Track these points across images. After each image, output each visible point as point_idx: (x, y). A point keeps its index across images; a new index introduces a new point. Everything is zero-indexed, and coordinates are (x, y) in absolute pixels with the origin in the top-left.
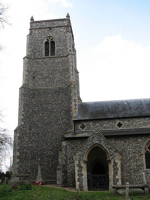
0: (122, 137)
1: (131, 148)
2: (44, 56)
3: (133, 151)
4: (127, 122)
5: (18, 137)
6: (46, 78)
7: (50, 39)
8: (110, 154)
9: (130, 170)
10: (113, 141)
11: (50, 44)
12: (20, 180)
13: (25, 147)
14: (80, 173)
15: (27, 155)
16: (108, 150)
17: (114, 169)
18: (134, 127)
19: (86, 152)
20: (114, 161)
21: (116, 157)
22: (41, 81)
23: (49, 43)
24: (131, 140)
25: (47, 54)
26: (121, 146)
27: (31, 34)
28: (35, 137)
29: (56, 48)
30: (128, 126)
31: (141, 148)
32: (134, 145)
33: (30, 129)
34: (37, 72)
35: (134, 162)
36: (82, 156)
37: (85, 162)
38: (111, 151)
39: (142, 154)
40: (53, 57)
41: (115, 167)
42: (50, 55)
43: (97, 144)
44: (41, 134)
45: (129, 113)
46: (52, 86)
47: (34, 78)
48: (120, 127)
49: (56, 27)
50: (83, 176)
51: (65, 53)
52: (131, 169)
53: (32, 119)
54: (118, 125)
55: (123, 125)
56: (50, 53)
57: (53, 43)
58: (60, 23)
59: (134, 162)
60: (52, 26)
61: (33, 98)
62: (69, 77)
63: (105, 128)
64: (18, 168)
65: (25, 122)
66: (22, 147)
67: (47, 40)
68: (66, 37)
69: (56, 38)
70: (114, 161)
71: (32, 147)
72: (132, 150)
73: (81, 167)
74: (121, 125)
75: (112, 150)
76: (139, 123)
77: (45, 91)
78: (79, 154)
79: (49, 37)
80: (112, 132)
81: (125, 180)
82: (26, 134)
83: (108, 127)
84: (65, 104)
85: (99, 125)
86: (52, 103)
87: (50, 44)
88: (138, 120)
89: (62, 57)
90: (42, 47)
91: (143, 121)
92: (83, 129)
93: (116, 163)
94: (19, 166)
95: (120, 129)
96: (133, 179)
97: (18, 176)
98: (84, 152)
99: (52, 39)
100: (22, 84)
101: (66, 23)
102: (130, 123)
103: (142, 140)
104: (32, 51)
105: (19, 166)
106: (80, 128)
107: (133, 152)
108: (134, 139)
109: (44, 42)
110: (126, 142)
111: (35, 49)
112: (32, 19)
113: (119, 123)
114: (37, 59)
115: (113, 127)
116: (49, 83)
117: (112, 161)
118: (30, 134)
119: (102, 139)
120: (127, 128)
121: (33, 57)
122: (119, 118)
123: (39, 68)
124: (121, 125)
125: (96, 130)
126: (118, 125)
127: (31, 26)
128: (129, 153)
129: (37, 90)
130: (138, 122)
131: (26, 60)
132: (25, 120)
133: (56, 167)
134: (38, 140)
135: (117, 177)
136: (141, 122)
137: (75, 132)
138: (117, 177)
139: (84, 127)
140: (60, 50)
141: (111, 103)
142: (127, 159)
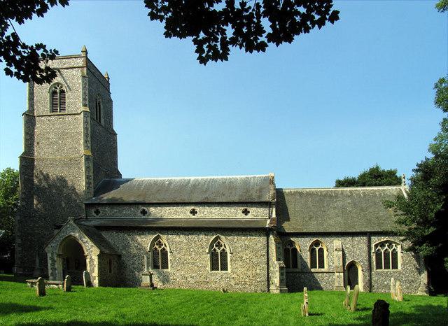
37: (59, 256)
49: (67, 68)
54: (141, 212)
60: (60, 67)
63: (125, 215)
73: (54, 261)
77: (54, 160)
80: (179, 222)
83: (129, 215)
95: (143, 217)
106: (94, 214)
115: (257, 212)
126: (141, 212)
133: (399, 280)
137: (87, 218)
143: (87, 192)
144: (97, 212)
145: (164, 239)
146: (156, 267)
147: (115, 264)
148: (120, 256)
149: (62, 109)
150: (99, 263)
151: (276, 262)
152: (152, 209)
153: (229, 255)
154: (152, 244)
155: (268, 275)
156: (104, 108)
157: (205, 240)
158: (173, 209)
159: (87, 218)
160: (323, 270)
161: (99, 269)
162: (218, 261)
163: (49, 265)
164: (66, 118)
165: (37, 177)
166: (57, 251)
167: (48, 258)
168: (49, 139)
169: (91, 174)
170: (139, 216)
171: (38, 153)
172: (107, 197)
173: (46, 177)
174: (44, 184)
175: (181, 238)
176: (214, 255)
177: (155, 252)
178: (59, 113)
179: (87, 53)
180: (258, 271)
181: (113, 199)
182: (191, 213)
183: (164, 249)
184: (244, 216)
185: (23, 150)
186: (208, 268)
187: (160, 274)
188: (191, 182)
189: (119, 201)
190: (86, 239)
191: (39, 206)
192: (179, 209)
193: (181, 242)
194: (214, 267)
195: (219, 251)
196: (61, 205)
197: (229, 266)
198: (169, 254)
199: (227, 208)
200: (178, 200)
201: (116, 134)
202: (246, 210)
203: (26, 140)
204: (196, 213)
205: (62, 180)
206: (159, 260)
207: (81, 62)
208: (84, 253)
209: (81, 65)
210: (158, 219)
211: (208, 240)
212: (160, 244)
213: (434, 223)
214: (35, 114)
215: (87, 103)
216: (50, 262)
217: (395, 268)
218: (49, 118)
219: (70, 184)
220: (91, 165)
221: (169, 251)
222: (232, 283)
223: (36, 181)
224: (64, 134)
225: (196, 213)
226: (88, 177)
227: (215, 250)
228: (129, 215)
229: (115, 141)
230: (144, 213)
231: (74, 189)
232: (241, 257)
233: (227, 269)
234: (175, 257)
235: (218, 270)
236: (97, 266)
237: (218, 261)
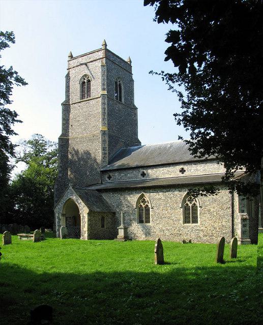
37: (63, 215)
49: (90, 62)
54: (142, 175)
77: (82, 138)
80: (201, 178)
126: (142, 175)
137: (102, 183)
143: (103, 161)
144: (109, 178)
145: (147, 196)
146: (141, 221)
147: (108, 220)
148: (114, 213)
149: (89, 95)
150: (89, 220)
151: (239, 214)
152: (150, 171)
154: (138, 202)
155: (233, 227)
156: (125, 87)
157: (179, 195)
158: (165, 169)
161: (89, 225)
162: (190, 215)
163: (57, 222)
164: (91, 102)
165: (71, 153)
166: (61, 211)
169: (107, 146)
170: (140, 178)
171: (72, 134)
172: (118, 164)
173: (77, 152)
174: (75, 157)
175: (160, 195)
176: (186, 209)
177: (140, 208)
178: (86, 99)
179: (106, 45)
180: (224, 223)
181: (123, 165)
182: (180, 171)
183: (147, 206)
184: (181, 175)
185: (60, 133)
186: (181, 222)
187: (144, 227)
189: (126, 167)
190: (80, 201)
191: (72, 176)
192: (171, 169)
193: (160, 199)
194: (186, 220)
195: (190, 205)
196: (86, 174)
197: (199, 219)
198: (151, 210)
199: (210, 164)
200: (170, 161)
203: (63, 124)
204: (185, 171)
205: (88, 153)
206: (143, 216)
207: (101, 54)
210: (154, 179)
211: (181, 195)
212: (144, 201)
214: (70, 103)
215: (105, 87)
216: (57, 220)
218: (79, 104)
219: (93, 155)
220: (107, 138)
221: (198, 206)
222: (201, 234)
223: (70, 156)
224: (90, 115)
225: (185, 171)
226: (104, 149)
227: (187, 204)
229: (136, 115)
230: (143, 175)
231: (95, 160)
232: (209, 211)
234: (155, 212)
235: (189, 222)
236: (87, 222)
237: (190, 215)
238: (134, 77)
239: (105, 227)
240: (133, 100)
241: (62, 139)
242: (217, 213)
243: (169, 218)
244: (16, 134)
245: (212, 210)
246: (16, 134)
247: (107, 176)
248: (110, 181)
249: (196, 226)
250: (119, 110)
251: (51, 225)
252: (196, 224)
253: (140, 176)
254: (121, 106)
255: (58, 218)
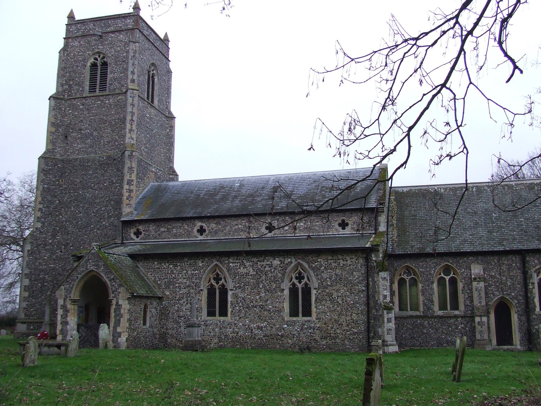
0: (172, 258)
1: (184, 278)
2: (86, 94)
3: (186, 283)
4: (214, 226)
5: (28, 251)
6: (87, 136)
7: (99, 56)
8: (112, 289)
9: (179, 317)
10: (156, 263)
11: (99, 67)
12: (28, 328)
13: (42, 271)
14: (64, 320)
15: (46, 284)
16: (108, 283)
17: (115, 316)
18: (225, 234)
19: (76, 283)
20: (117, 303)
21: (120, 295)
22: (78, 144)
23: (97, 66)
24: (186, 263)
25: (92, 88)
26: (168, 273)
27: (66, 45)
28: (61, 252)
29: (110, 76)
30: (216, 232)
31: (201, 278)
32: (189, 272)
33: (54, 236)
34: (72, 126)
35: (187, 303)
36: (68, 291)
38: (114, 283)
39: (202, 290)
40: (102, 96)
41: (118, 313)
42: (97, 90)
43: (92, 271)
44: (71, 247)
45: (227, 206)
46: (96, 153)
47: (66, 137)
48: (201, 235)
49: (112, 32)
50: (68, 326)
51: (123, 86)
52: (181, 317)
53: (57, 218)
54: (198, 231)
55: (207, 232)
56: (98, 87)
57: (105, 64)
58: (120, 24)
59: (187, 303)
61: (61, 176)
62: (124, 136)
64: (25, 308)
65: (43, 223)
66: (35, 269)
67: (96, 59)
68: (128, 52)
69: (110, 53)
70: (117, 303)
71: (54, 269)
72: (185, 281)
73: (66, 311)
74: (205, 231)
75: (116, 282)
76: (236, 227)
78: (65, 288)
79: (98, 53)
81: (169, 336)
82: (45, 245)
84: (116, 188)
85: (166, 230)
86: (94, 186)
87: (99, 67)
88: (235, 223)
89: (118, 94)
90: (83, 74)
91: (244, 224)
92: (137, 237)
93: (120, 305)
94: (27, 305)
95: (201, 238)
96: (182, 333)
97: (24, 323)
98: (73, 285)
99: (104, 58)
100: (45, 150)
101: (130, 22)
102: (220, 227)
103: (204, 264)
104: (67, 83)
105: (27, 305)
106: (133, 236)
107: (187, 284)
108: (192, 261)
109: (89, 64)
110: (177, 266)
111: (71, 79)
112: (71, 16)
113: (201, 227)
114: (73, 99)
116: (91, 146)
117: (114, 302)
118: (53, 246)
119: (100, 263)
120: (213, 237)
121: (66, 96)
122: (200, 218)
123: (75, 117)
124: (205, 231)
125: (93, 248)
126: (198, 231)
127: (68, 31)
128: (180, 286)
129: (69, 161)
130: (234, 226)
131: (53, 102)
132: (45, 219)
134: (66, 256)
135: (119, 330)
136: (240, 226)
138: (119, 330)
139: (141, 233)
140: (115, 80)
141: (214, 181)
142: (175, 297)
144: (138, 234)
149: (103, 88)
153: (314, 292)
159: (122, 243)
160: (456, 312)
167: (59, 307)
168: (81, 130)
180: (355, 317)
183: (223, 285)
188: (270, 182)
193: (247, 274)
197: (314, 309)
201: (173, 118)
202: (343, 221)
208: (108, 296)
209: (130, 27)
213: (304, 228)
217: (212, 316)
228: (181, 236)
233: (310, 315)
238: (172, 66)
239: (148, 324)
240: (169, 103)
241: (46, 158)
242: (343, 300)
243: (262, 307)
244: (386, 83)
245: (335, 295)
246: (386, 83)
247: (133, 230)
248: (137, 240)
249: (309, 321)
250: (151, 119)
251: (292, 316)
252: (309, 318)
253: (264, 230)
254: (153, 111)
255: (64, 307)
